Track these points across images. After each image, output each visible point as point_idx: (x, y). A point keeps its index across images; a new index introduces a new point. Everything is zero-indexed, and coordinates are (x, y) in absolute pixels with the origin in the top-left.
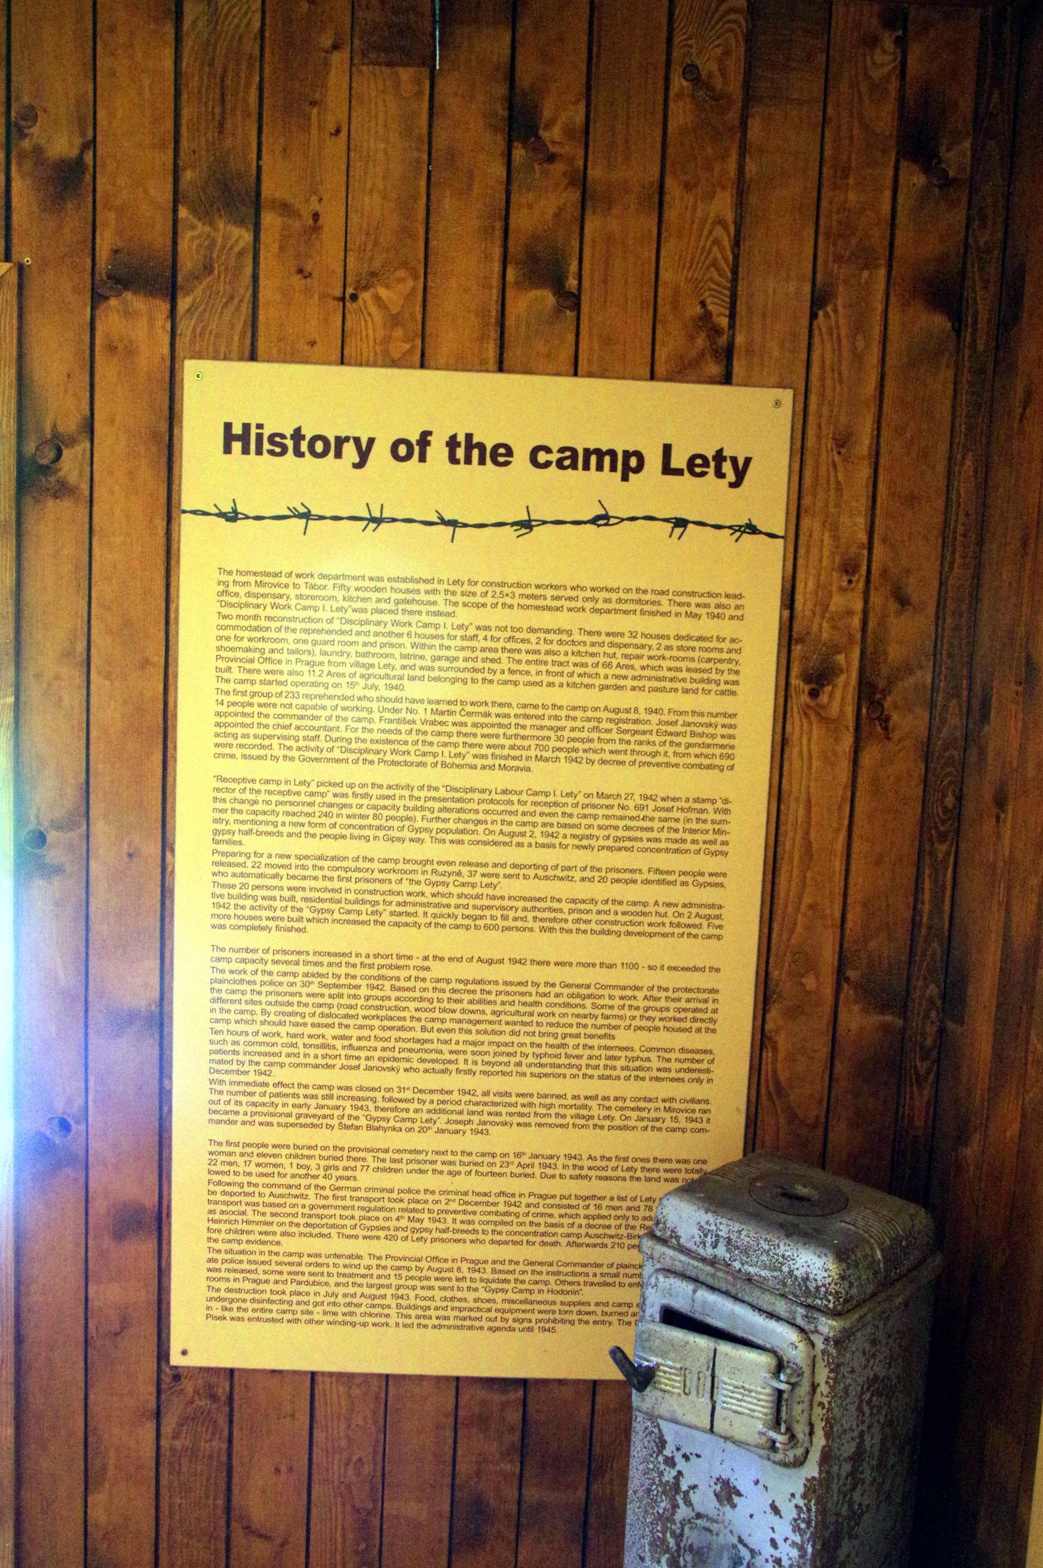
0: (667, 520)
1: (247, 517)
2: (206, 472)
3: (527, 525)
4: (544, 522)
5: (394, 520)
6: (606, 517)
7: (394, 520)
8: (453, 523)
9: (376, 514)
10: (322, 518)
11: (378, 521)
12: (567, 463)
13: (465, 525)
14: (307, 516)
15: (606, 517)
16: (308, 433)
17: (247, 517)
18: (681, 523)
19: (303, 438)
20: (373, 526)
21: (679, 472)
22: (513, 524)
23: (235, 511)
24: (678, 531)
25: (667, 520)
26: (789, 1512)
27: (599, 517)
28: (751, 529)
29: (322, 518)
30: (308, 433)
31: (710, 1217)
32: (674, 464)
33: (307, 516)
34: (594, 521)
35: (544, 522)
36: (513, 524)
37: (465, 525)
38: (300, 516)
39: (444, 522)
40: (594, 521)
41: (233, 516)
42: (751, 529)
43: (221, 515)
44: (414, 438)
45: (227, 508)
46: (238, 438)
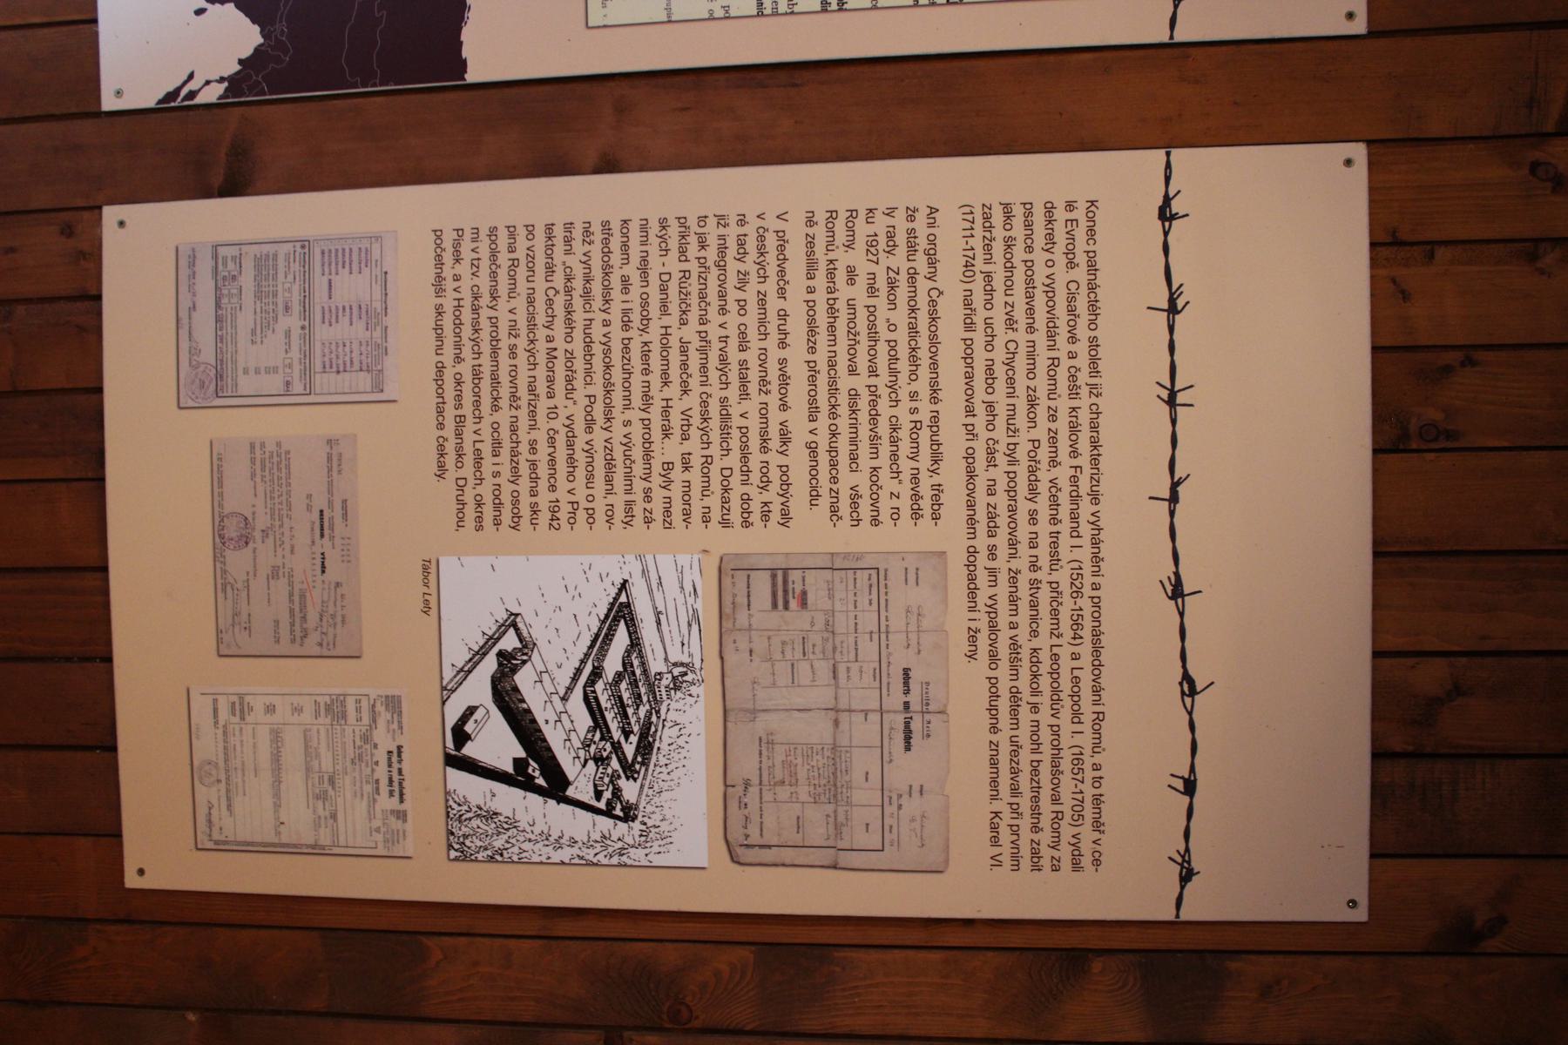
0: (1192, 769)
1: (1166, 234)
3: (1177, 592)
4: (1182, 614)
5: (1174, 422)
6: (1193, 692)
7: (1174, 422)
8: (1174, 498)
9: (1180, 398)
10: (1171, 329)
11: (1171, 402)
13: (1172, 513)
14: (1173, 310)
15: (1193, 692)
17: (1166, 234)
18: (1190, 787)
20: (1165, 394)
22: (1177, 574)
23: (1173, 217)
24: (1180, 784)
25: (1192, 769)
27: (1191, 682)
28: (1187, 876)
29: (1171, 329)
33: (1173, 310)
34: (1187, 677)
35: (1182, 614)
36: (1177, 574)
37: (1172, 513)
40: (1187, 677)
42: (1187, 876)
43: (1167, 200)
45: (1176, 206)
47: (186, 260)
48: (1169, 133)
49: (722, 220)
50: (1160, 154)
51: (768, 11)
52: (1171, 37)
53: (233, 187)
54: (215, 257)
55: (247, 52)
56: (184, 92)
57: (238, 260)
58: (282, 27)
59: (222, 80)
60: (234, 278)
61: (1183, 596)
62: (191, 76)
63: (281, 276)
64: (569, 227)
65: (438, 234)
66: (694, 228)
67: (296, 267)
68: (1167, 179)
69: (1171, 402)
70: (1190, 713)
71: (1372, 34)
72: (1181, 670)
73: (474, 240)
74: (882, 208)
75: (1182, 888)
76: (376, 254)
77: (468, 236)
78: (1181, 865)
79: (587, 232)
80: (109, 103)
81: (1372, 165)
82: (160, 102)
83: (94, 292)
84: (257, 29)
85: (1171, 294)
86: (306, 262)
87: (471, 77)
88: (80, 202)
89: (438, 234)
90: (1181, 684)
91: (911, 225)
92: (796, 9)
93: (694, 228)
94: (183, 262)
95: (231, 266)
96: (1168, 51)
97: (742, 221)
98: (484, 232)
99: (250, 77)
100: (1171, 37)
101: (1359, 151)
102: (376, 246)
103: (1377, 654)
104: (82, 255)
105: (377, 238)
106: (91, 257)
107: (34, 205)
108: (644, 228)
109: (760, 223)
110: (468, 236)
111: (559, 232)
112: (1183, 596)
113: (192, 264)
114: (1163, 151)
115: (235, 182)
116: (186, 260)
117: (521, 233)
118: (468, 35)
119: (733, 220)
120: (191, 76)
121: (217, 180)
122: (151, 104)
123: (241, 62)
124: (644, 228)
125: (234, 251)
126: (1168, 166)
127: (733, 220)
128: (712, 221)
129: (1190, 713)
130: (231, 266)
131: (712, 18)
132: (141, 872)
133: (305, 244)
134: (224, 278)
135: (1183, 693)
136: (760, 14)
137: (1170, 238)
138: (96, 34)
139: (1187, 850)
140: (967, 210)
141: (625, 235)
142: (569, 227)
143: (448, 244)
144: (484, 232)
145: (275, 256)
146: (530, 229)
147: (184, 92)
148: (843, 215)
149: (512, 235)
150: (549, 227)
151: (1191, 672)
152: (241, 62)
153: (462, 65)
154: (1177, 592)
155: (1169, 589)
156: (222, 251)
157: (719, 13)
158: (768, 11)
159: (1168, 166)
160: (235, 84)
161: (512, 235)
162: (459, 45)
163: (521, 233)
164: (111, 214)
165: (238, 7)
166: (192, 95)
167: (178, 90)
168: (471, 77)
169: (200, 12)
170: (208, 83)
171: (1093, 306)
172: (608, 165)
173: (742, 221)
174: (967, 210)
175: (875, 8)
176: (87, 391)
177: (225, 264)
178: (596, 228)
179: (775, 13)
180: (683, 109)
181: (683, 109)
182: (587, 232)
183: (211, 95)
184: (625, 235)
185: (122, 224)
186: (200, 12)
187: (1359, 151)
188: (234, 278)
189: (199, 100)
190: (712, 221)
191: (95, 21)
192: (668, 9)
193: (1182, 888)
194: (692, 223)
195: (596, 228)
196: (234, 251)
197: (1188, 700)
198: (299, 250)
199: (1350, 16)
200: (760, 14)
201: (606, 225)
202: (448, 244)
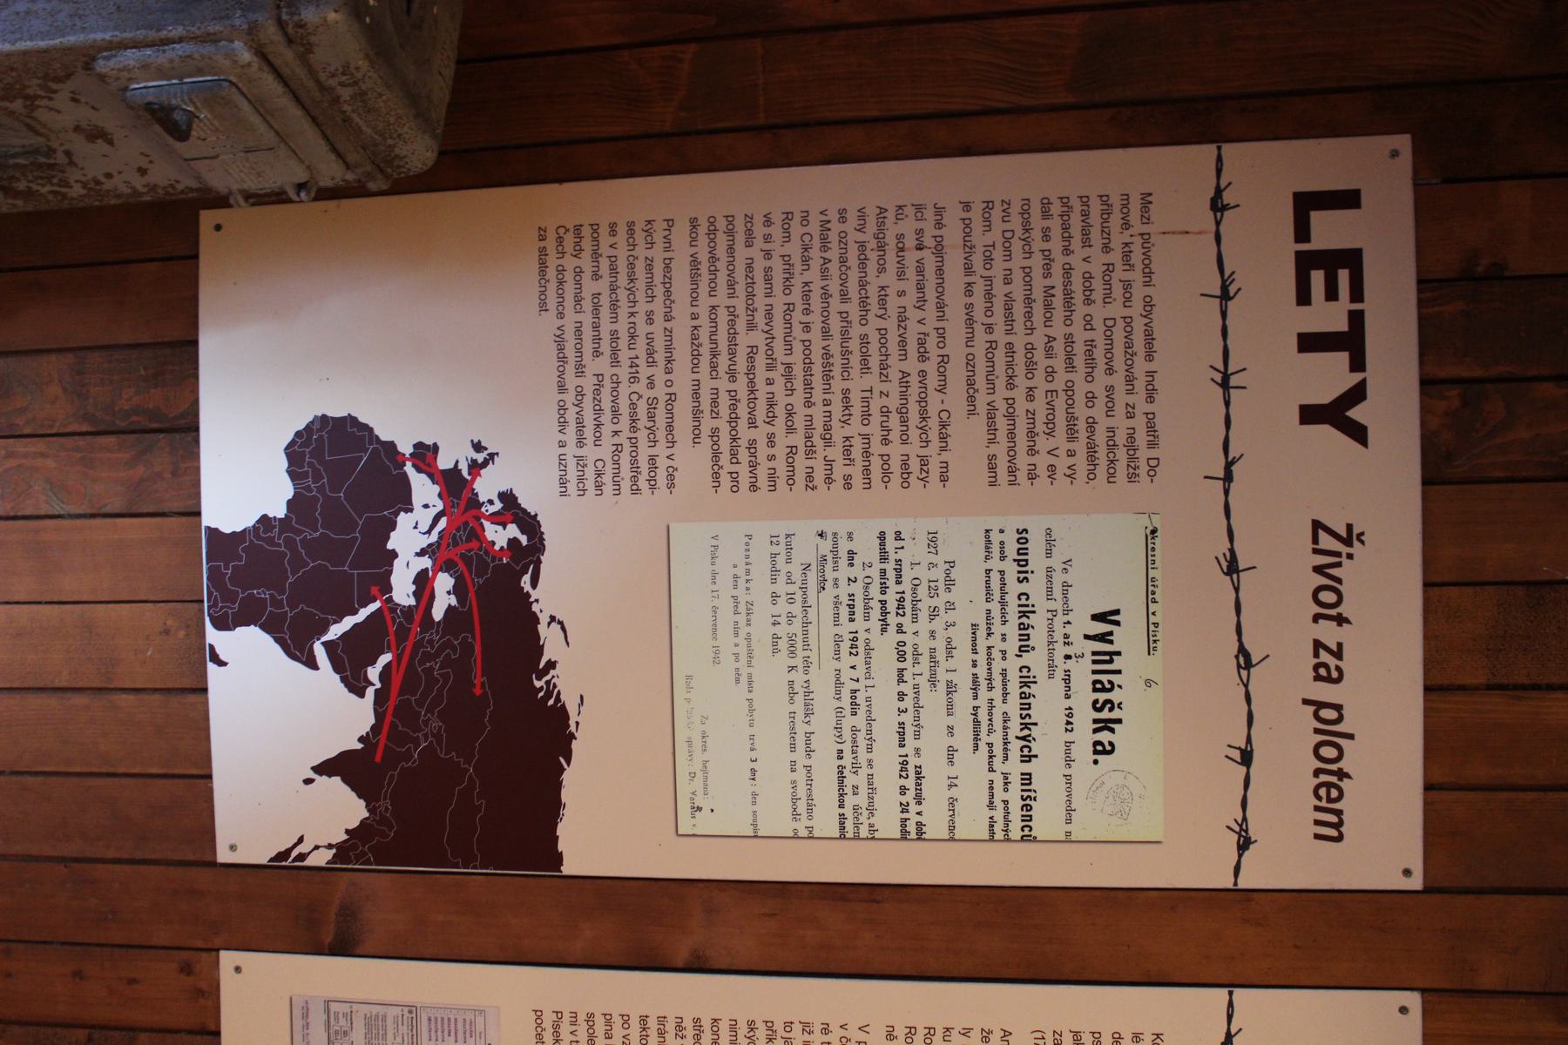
0: (1249, 740)
1: (1218, 223)
2: (1268, 171)
3: (1232, 568)
4: (1237, 590)
5: (1227, 404)
6: (1249, 665)
7: (1227, 404)
8: (1228, 477)
9: (1233, 381)
10: (1224, 314)
11: (1225, 384)
12: (1322, 672)
13: (1226, 492)
14: (1225, 296)
15: (1249, 665)
16: (1345, 784)
17: (1218, 223)
18: (1246, 758)
19: (1340, 779)
20: (1218, 377)
21: (1302, 233)
22: (1232, 551)
23: (1225, 208)
24: (1237, 755)
25: (1249, 740)
26: (139, 183)
27: (1247, 656)
28: (1244, 845)
29: (1224, 314)
30: (1345, 784)
31: (364, 65)
32: (1316, 217)
33: (1225, 296)
34: (1242, 650)
35: (1237, 590)
36: (1232, 551)
37: (1226, 492)
38: (1224, 288)
39: (1229, 466)
40: (1242, 650)
41: (1245, 660)
42: (1244, 845)
43: (1219, 192)
44: (1343, 609)
45: (1228, 197)
46: (1332, 828)
47: (299, 1012)
48: (1232, 978)
49: (807, 1027)
50: (1213, 148)
51: (850, 835)
52: (1236, 884)
53: (343, 947)
54: (328, 1011)
55: (354, 824)
56: (294, 854)
57: (350, 1016)
58: (385, 804)
59: (330, 846)
60: (345, 1033)
61: (1238, 572)
62: (301, 840)
63: (390, 1036)
64: (662, 1020)
65: (538, 1014)
66: (781, 1032)
67: (404, 1029)
68: (1230, 1017)
69: (1225, 384)
70: (1246, 686)
71: (1427, 890)
72: (1236, 645)
73: (573, 1023)
74: (958, 1028)
75: (1240, 856)
76: (480, 1026)
77: (566, 1018)
78: (1239, 834)
79: (679, 1027)
80: (224, 856)
81: (1426, 1013)
82: (271, 860)
83: (213, 1028)
84: (362, 803)
85: (1224, 281)
86: (414, 1025)
87: (567, 869)
88: (200, 944)
89: (538, 1014)
90: (1237, 657)
91: (969, 300)
92: (877, 835)
93: (781, 1032)
94: (297, 1013)
95: (342, 1022)
96: (1231, 895)
97: (826, 1030)
98: (582, 1017)
99: (353, 847)
100: (1236, 884)
101: (1413, 1000)
102: (480, 1020)
103: (1428, 787)
104: (200, 993)
105: (481, 1012)
106: (209, 995)
107: (155, 941)
108: (733, 1027)
109: (843, 1033)
110: (566, 1018)
111: (653, 1024)
112: (1238, 572)
113: (306, 1015)
114: (1225, 991)
115: (345, 944)
116: (299, 1012)
117: (618, 1021)
118: (560, 826)
119: (817, 1028)
120: (301, 840)
121: (328, 939)
122: (264, 861)
123: (347, 832)
124: (733, 1027)
125: (345, 1008)
126: (1219, 159)
127: (817, 1028)
128: (797, 1028)
129: (1246, 686)
130: (342, 1022)
131: (796, 837)
132: (218, 228)
133: (412, 1009)
134: (336, 1032)
135: (1239, 666)
136: (842, 837)
137: (1222, 228)
138: (211, 790)
139: (1245, 819)
140: (1039, 1035)
141: (715, 1033)
142: (662, 1020)
143: (548, 1023)
144: (582, 1017)
145: (384, 1018)
146: (625, 1018)
147: (294, 854)
148: (921, 1032)
149: (609, 1023)
150: (644, 1019)
151: (1247, 646)
152: (347, 832)
153: (558, 859)
154: (1232, 568)
155: (1225, 565)
156: (334, 1007)
157: (803, 833)
158: (850, 835)
159: (1219, 159)
160: (343, 851)
161: (609, 1023)
162: (555, 839)
163: (618, 1021)
164: (228, 959)
165: (345, 781)
166: (302, 857)
167: (289, 851)
168: (567, 869)
169: (308, 781)
170: (317, 847)
171: (1149, 338)
172: (698, 965)
173: (826, 1030)
174: (1039, 1035)
175: (952, 839)
176: (194, 691)
177: (337, 1019)
178: (688, 1024)
179: (857, 838)
180: (765, 915)
181: (765, 915)
182: (679, 1027)
183: (321, 858)
184: (715, 1033)
185: (238, 969)
186: (308, 781)
187: (1413, 1000)
188: (345, 1033)
189: (309, 862)
190: (797, 1028)
191: (209, 777)
192: (755, 825)
193: (1240, 856)
194: (779, 1026)
195: (688, 1024)
196: (345, 1008)
197: (1244, 673)
198: (407, 1014)
199: (1403, 1010)
200: (842, 837)
201: (697, 1021)
202: (548, 1023)
